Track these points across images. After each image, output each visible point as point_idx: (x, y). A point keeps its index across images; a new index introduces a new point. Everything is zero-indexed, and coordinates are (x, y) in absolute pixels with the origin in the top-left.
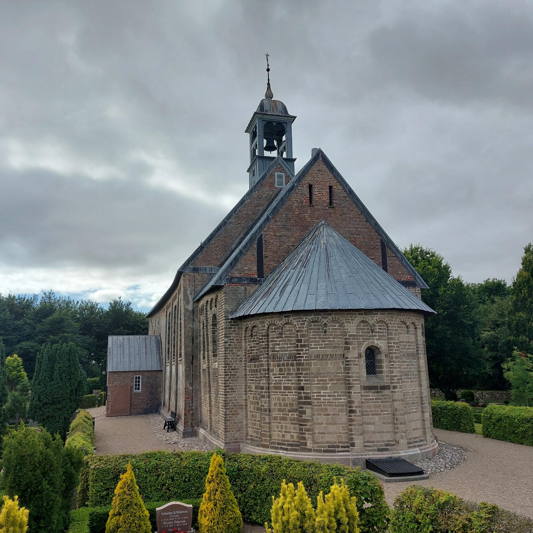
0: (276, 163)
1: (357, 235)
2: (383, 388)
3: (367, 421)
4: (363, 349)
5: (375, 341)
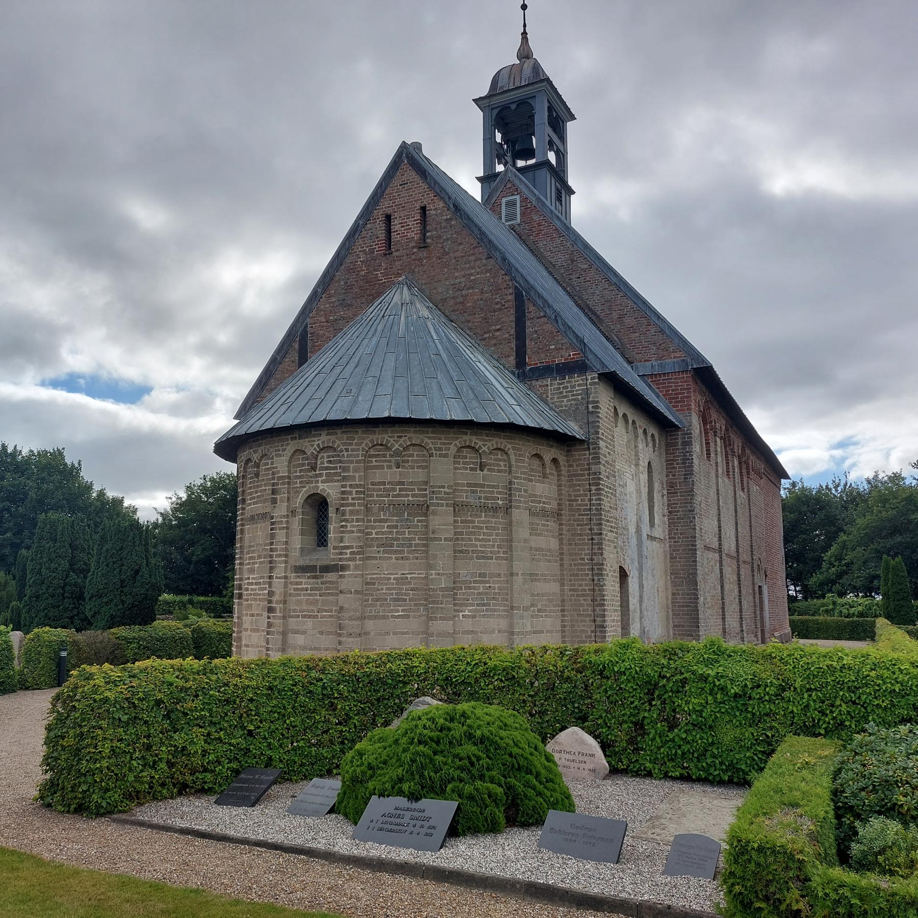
0: (502, 179)
1: (469, 289)
2: (326, 569)
3: (295, 627)
4: (299, 500)
5: (320, 484)
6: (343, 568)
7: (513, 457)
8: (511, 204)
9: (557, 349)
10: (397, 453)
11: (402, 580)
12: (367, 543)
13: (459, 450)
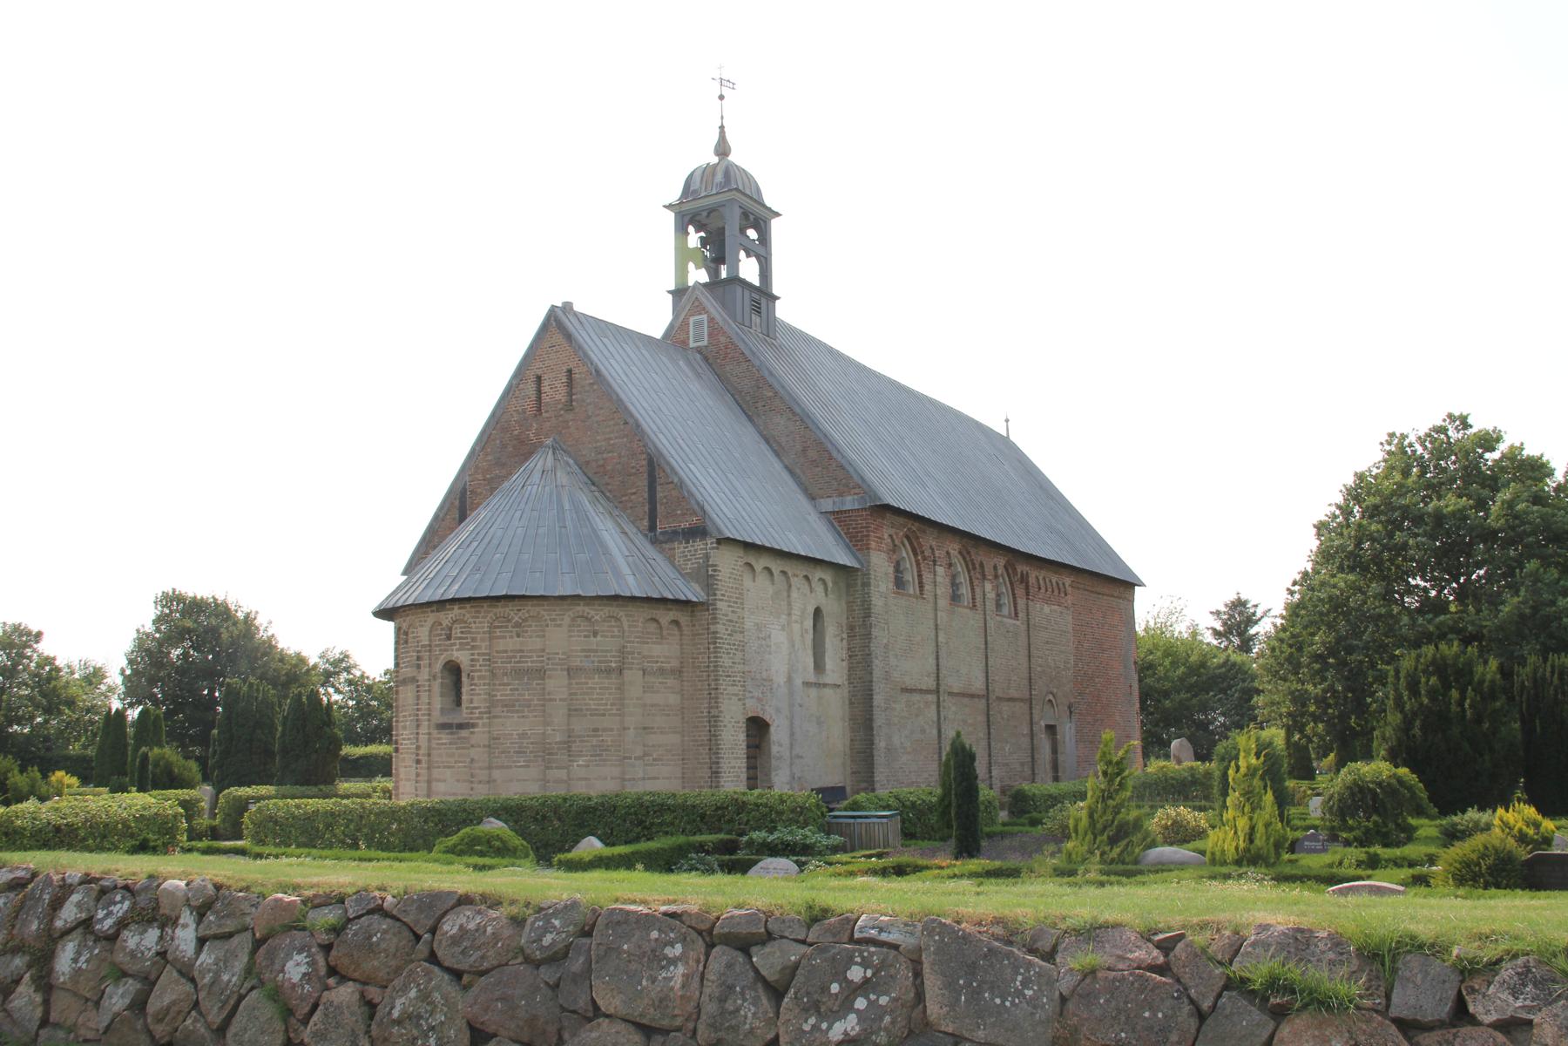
2: (461, 726)
4: (438, 666)
6: (473, 725)
7: (626, 625)
8: (698, 324)
9: (683, 514)
10: (518, 625)
11: (523, 735)
12: (492, 703)
13: (573, 620)
